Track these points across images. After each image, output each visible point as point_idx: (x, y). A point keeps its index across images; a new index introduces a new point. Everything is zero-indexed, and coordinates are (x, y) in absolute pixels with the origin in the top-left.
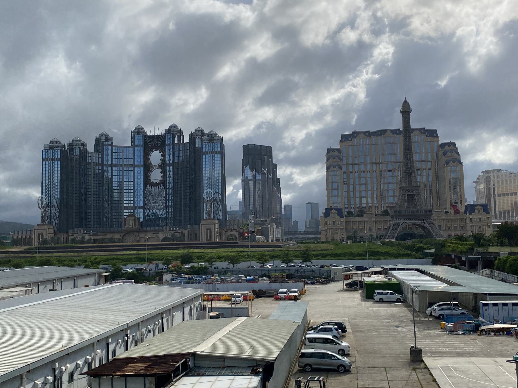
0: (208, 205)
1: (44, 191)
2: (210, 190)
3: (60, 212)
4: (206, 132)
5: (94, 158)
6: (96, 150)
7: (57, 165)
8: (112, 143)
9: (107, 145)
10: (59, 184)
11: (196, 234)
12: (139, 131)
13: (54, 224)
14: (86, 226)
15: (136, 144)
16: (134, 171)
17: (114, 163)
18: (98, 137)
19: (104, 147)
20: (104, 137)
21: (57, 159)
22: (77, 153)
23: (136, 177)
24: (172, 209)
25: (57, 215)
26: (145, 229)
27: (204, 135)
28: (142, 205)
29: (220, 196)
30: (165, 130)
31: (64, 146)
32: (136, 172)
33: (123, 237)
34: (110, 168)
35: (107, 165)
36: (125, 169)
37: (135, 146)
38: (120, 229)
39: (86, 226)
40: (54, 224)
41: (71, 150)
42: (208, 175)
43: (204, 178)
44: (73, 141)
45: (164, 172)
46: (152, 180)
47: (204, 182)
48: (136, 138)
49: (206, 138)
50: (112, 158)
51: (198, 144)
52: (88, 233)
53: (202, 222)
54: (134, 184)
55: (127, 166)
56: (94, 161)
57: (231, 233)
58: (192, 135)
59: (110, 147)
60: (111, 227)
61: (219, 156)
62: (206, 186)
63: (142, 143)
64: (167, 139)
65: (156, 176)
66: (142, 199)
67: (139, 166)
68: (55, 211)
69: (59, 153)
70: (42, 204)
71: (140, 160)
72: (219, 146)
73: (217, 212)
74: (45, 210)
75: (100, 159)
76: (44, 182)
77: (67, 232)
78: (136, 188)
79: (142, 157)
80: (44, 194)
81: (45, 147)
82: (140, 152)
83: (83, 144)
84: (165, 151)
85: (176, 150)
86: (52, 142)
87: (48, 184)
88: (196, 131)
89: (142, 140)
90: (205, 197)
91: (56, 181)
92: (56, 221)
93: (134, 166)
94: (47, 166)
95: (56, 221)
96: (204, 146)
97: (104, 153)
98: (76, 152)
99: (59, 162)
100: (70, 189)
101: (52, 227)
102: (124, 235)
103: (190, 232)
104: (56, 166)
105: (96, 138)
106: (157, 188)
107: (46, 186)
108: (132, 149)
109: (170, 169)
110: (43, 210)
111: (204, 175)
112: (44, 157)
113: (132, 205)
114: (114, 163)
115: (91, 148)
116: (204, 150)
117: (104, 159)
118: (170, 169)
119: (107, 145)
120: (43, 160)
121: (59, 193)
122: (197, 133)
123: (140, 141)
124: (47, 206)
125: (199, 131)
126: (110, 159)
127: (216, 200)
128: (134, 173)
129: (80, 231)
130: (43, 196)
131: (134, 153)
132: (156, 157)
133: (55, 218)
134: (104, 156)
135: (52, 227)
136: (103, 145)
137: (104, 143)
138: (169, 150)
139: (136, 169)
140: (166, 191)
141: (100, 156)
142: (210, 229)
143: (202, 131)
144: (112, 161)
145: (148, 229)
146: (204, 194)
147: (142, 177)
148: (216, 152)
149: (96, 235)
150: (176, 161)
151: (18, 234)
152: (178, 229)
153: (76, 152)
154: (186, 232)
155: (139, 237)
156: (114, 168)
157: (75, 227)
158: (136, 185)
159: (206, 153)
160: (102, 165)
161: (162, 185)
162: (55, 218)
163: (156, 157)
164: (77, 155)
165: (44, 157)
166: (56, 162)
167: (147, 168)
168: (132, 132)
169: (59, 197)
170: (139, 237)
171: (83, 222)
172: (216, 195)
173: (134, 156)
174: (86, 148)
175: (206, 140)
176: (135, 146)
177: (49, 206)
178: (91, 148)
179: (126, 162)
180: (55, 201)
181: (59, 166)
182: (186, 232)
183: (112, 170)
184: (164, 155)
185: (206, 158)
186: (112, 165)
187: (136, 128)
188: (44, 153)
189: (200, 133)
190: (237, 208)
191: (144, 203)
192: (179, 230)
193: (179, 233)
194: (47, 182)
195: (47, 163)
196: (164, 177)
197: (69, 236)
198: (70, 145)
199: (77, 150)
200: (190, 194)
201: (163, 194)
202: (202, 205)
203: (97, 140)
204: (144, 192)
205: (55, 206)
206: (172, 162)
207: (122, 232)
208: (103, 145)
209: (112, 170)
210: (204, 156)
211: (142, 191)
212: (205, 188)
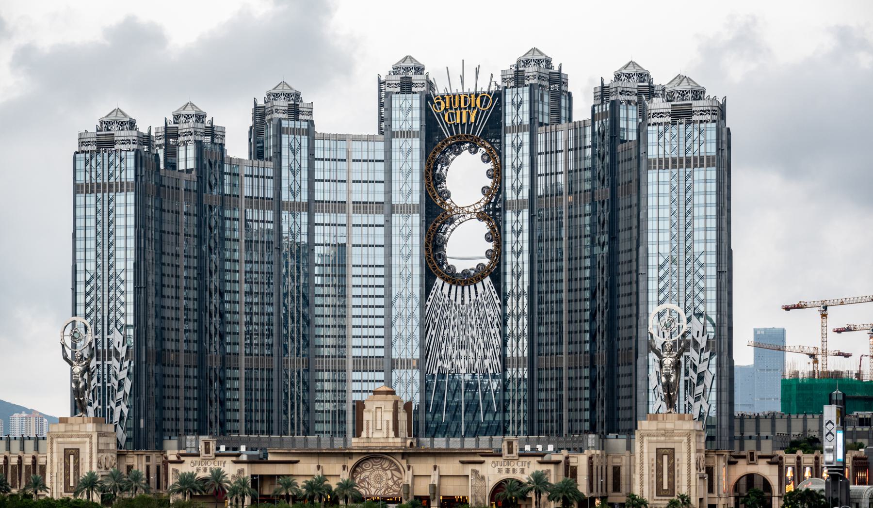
0: (668, 361)
1: (81, 299)
2: (674, 306)
3: (136, 376)
4: (661, 78)
5: (247, 181)
6: (258, 153)
7: (125, 206)
8: (311, 123)
9: (295, 131)
10: (131, 276)
11: (617, 471)
12: (406, 78)
13: (116, 418)
14: (222, 425)
15: (395, 126)
16: (388, 223)
17: (318, 197)
18: (261, 103)
19: (285, 139)
20: (282, 103)
21: (122, 187)
22: (191, 165)
23: (395, 251)
24: (523, 373)
25: (128, 385)
26: (426, 441)
27: (650, 92)
28: (417, 355)
29: (710, 328)
30: (504, 72)
31: (146, 140)
32: (395, 231)
33: (354, 470)
34: (304, 217)
35: (295, 208)
36: (357, 219)
37: (394, 135)
38: (338, 443)
39: (222, 425)
40: (116, 418)
41: (171, 153)
42: (665, 249)
43: (653, 261)
44: (177, 117)
45: (497, 236)
46: (450, 262)
47: (653, 273)
48: (395, 104)
49: (658, 104)
50: (311, 180)
51: (629, 120)
52: (233, 452)
53: (644, 425)
54: (388, 276)
55: (362, 207)
56: (247, 192)
57: (751, 469)
58: (604, 93)
59: (304, 140)
60: (307, 432)
61: (712, 173)
62: (660, 291)
63: (416, 126)
64: (509, 108)
65: (467, 245)
66: (417, 333)
67: (406, 210)
68: (121, 371)
69: (131, 163)
70: (74, 346)
71: (409, 188)
72: (712, 135)
73: (699, 390)
74: (87, 369)
75: (270, 183)
76: (80, 267)
77: (160, 448)
78: (395, 291)
79: (416, 176)
80: (80, 310)
81: (82, 143)
82: (409, 156)
83: (211, 131)
84: (501, 153)
85: (541, 148)
86: (106, 124)
87: (96, 276)
88: (618, 77)
89: (416, 114)
90: (654, 332)
91: (120, 266)
92: (123, 406)
93: (387, 208)
94: (91, 212)
95: (123, 406)
96: (652, 138)
97: (285, 163)
98: (187, 158)
99: (131, 197)
100: (168, 292)
101: (111, 428)
102: (357, 465)
103: (595, 460)
104: (120, 210)
105: (256, 108)
106: (469, 292)
107: (87, 283)
108: (380, 145)
109: (517, 222)
110: (78, 369)
111: (652, 249)
112: (80, 178)
113: (381, 352)
114: (318, 197)
115: (237, 147)
116: (653, 152)
117: (285, 185)
118: (517, 222)
119: (295, 131)
120: (78, 189)
121: (130, 309)
122: (625, 84)
123: (408, 113)
124: (94, 352)
125: (629, 76)
126: (305, 186)
127: (696, 344)
128: (388, 235)
129: (510, 443)
130: (80, 320)
131: (388, 160)
132: (466, 177)
133: (120, 395)
134: (285, 173)
135: (111, 428)
136: (280, 130)
137: (285, 124)
138: (516, 148)
139: (396, 219)
140: (505, 303)
141: (270, 172)
142: (76, 453)
143: (643, 76)
144: (311, 190)
145: (440, 443)
146: (653, 321)
147: (417, 251)
148: (701, 162)
149: (263, 461)
150: (540, 192)
151: (23, 448)
152: (551, 448)
153: (187, 158)
154: (581, 462)
155: (409, 473)
156: (318, 218)
157: (187, 432)
158: (395, 281)
159: (664, 164)
160: (277, 204)
161: (487, 280)
162: (120, 395)
163: (466, 177)
164: (189, 171)
165: (80, 178)
166: (120, 198)
167: (436, 214)
168: (381, 83)
169: (130, 321)
170: (409, 473)
171: (210, 419)
172: (697, 325)
173: (389, 172)
174: (222, 145)
175: (661, 115)
176: (394, 135)
177: (101, 352)
178: (237, 147)
179: (359, 193)
180: (117, 337)
181: (131, 210)
182: (581, 462)
183: (311, 224)
184: (498, 174)
185: (658, 186)
186: (311, 206)
187: (396, 70)
188: (81, 165)
189: (633, 84)
190: (491, 181)
191: (422, 345)
192: (558, 450)
193: (557, 463)
194: (91, 266)
195: (91, 199)
196: (497, 255)
197: (166, 462)
198: (170, 133)
199: (191, 152)
200: (593, 316)
201: (492, 313)
202: (641, 361)
203: (260, 114)
204: (423, 307)
205: (117, 354)
206: (525, 194)
207: (350, 455)
208: (280, 130)
209: (311, 224)
210: (652, 176)
211: (415, 303)
212: (653, 297)
